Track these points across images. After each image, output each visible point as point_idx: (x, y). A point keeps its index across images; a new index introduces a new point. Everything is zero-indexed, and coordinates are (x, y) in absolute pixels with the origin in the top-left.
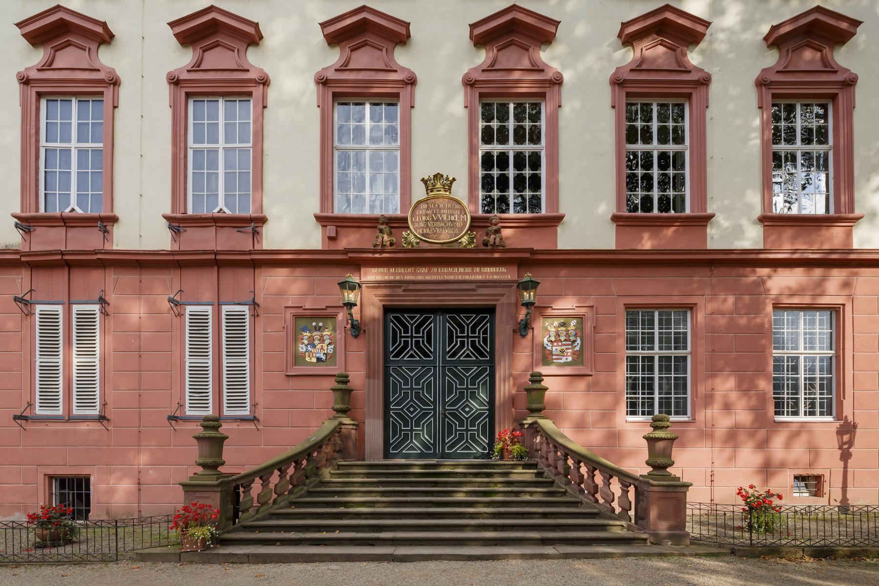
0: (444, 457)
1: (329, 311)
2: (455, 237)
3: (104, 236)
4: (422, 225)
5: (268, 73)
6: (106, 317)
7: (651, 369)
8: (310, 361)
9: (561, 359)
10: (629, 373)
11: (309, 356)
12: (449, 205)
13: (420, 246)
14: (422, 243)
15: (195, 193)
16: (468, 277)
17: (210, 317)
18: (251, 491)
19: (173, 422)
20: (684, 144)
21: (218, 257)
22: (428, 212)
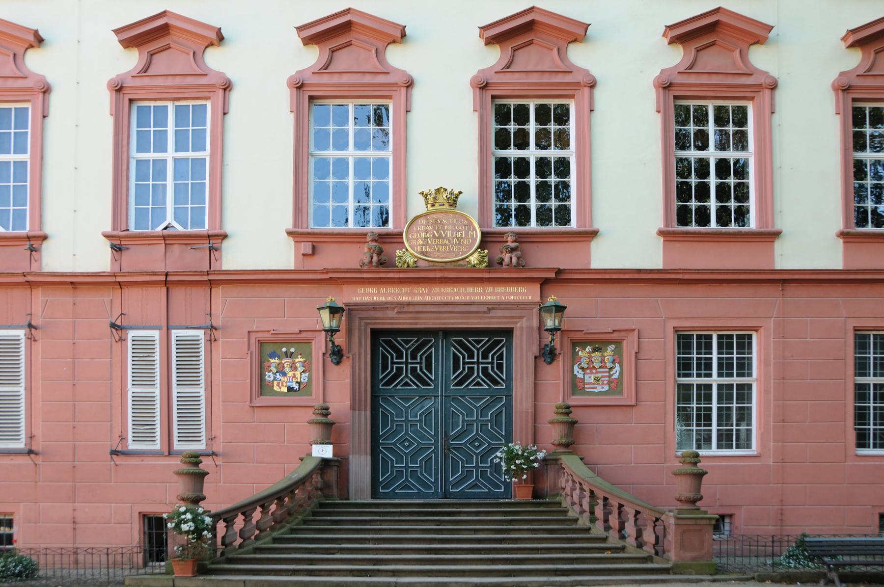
0: (448, 496)
1: (303, 335)
2: (461, 255)
3: (31, 254)
4: (420, 242)
5: (229, 77)
6: (33, 343)
7: (709, 398)
8: (279, 390)
9: (595, 388)
10: (878, 351)
11: (278, 385)
12: (455, 221)
13: (418, 265)
14: (420, 261)
15: (138, 206)
16: (478, 298)
17: (157, 342)
18: (234, 526)
19: (114, 456)
20: (748, 150)
21: (169, 278)
22: (428, 228)
